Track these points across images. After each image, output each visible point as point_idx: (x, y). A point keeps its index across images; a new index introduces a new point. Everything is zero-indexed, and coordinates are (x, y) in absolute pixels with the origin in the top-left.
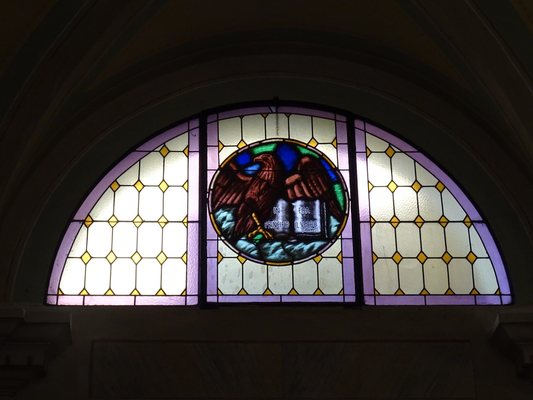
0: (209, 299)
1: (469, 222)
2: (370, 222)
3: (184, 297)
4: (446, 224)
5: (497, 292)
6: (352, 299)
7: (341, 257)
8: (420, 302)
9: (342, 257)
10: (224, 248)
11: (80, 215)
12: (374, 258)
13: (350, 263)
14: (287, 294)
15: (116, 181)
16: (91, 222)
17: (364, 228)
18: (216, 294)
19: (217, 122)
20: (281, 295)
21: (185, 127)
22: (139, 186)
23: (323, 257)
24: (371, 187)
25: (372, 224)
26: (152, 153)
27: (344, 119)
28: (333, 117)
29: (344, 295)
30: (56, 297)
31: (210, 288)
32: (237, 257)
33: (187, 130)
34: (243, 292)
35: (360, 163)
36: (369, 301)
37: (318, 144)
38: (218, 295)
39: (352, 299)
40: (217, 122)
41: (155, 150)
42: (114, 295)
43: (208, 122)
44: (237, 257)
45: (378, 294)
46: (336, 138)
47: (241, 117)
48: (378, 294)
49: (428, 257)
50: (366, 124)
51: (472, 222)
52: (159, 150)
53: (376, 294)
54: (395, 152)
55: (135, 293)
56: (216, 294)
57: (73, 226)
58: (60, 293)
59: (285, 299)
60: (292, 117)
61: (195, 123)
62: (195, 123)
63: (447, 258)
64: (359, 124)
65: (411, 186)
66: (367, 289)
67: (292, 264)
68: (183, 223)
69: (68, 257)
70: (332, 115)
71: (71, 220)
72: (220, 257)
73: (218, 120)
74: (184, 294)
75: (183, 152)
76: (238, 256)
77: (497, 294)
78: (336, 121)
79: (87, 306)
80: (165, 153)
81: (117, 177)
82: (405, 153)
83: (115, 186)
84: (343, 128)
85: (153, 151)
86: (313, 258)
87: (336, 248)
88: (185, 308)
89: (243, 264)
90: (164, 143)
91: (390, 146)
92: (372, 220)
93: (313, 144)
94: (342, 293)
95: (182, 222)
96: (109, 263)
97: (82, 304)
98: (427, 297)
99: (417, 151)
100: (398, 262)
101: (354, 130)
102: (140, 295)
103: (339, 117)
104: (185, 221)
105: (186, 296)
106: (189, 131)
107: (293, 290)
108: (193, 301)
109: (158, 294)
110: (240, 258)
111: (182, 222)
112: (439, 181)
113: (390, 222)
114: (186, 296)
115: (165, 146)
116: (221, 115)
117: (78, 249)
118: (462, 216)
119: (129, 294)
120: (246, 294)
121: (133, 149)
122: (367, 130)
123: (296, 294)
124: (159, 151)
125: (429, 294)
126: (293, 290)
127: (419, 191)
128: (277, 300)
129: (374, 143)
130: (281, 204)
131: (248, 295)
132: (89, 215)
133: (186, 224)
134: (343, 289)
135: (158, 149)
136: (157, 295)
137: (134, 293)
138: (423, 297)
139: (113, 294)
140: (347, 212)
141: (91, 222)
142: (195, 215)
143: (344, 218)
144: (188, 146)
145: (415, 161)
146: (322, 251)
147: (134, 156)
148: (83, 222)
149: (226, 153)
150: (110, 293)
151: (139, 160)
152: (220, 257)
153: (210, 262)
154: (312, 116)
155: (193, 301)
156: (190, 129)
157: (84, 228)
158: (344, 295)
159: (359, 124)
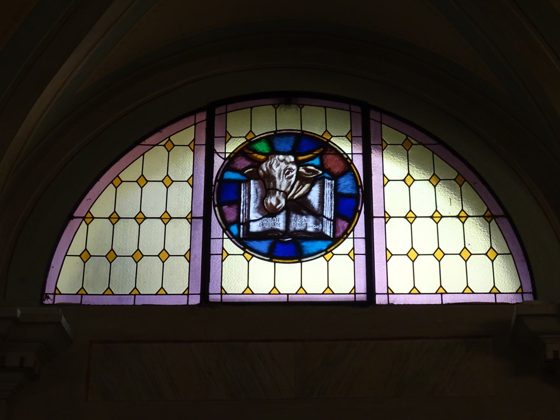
0: (212, 298)
1: (462, 217)
2: (385, 217)
3: (186, 296)
4: (439, 219)
5: (186, 292)
6: (363, 297)
7: (352, 255)
8: (490, 299)
9: (354, 254)
10: (230, 246)
11: (80, 211)
12: (188, 256)
13: (361, 260)
14: (295, 293)
15: (118, 176)
16: (90, 218)
17: (377, 223)
18: (386, 292)
19: (225, 114)
20: (288, 294)
21: (191, 119)
22: (142, 182)
23: (334, 254)
24: (386, 181)
25: (387, 219)
26: (155, 144)
27: (359, 109)
28: (348, 109)
29: (522, 293)
30: (357, 295)
31: (213, 288)
32: (243, 255)
33: (193, 123)
34: (415, 291)
35: (375, 158)
36: (380, 300)
37: (332, 136)
38: (221, 294)
39: (363, 297)
40: (225, 114)
41: (160, 144)
42: (420, 293)
43: (216, 113)
44: (243, 255)
45: (391, 292)
46: (351, 131)
47: (252, 108)
48: (391, 292)
49: (419, 254)
50: (205, 122)
51: (493, 217)
52: (163, 144)
53: (389, 292)
54: (413, 144)
55: (441, 291)
56: (386, 292)
57: (73, 223)
58: (57, 292)
59: (293, 298)
60: (305, 109)
61: (202, 116)
62: (202, 116)
63: (439, 254)
64: (374, 115)
65: (429, 180)
66: (380, 287)
67: (301, 262)
68: (187, 219)
69: (66, 255)
70: (347, 106)
71: (71, 217)
72: (224, 254)
73: (226, 113)
74: (186, 293)
75: (189, 146)
76: (244, 253)
77: (352, 293)
78: (350, 111)
79: (398, 305)
80: (170, 147)
81: (119, 173)
82: (424, 145)
83: (117, 182)
84: (359, 119)
85: (157, 145)
86: (323, 256)
87: (346, 246)
88: (188, 307)
89: (248, 261)
90: (169, 137)
91: (407, 138)
92: (387, 216)
93: (327, 137)
94: (353, 292)
95: (186, 218)
96: (246, 260)
97: (440, 303)
98: (443, 295)
99: (437, 143)
100: (413, 259)
101: (370, 122)
102: (446, 293)
103: (354, 108)
104: (189, 217)
105: (388, 294)
106: (195, 124)
107: (494, 288)
108: (195, 300)
109: (412, 292)
110: (246, 255)
111: (186, 218)
112: (112, 182)
113: (406, 217)
114: (388, 294)
115: (170, 140)
116: (230, 107)
117: (77, 247)
118: (455, 209)
119: (408, 292)
120: (471, 292)
121: (137, 143)
122: (383, 122)
123: (332, 293)
124: (164, 146)
125: (500, 293)
126: (494, 288)
127: (462, 184)
128: (284, 298)
129: (389, 134)
130: (282, 198)
131: (473, 293)
132: (89, 211)
133: (190, 220)
134: (188, 288)
135: (163, 143)
136: (244, 293)
137: (440, 291)
138: (440, 295)
139: (305, 293)
140: (359, 209)
141: (90, 218)
142: (200, 212)
143: (356, 215)
144: (194, 140)
145: (433, 153)
146: (333, 247)
147: (138, 150)
148: (84, 218)
149: (231, 147)
150: (415, 291)
151: (143, 155)
152: (225, 255)
153: (215, 261)
154: (325, 108)
155: (195, 300)
156: (197, 122)
157: (84, 224)
158: (355, 294)
159: (374, 115)
